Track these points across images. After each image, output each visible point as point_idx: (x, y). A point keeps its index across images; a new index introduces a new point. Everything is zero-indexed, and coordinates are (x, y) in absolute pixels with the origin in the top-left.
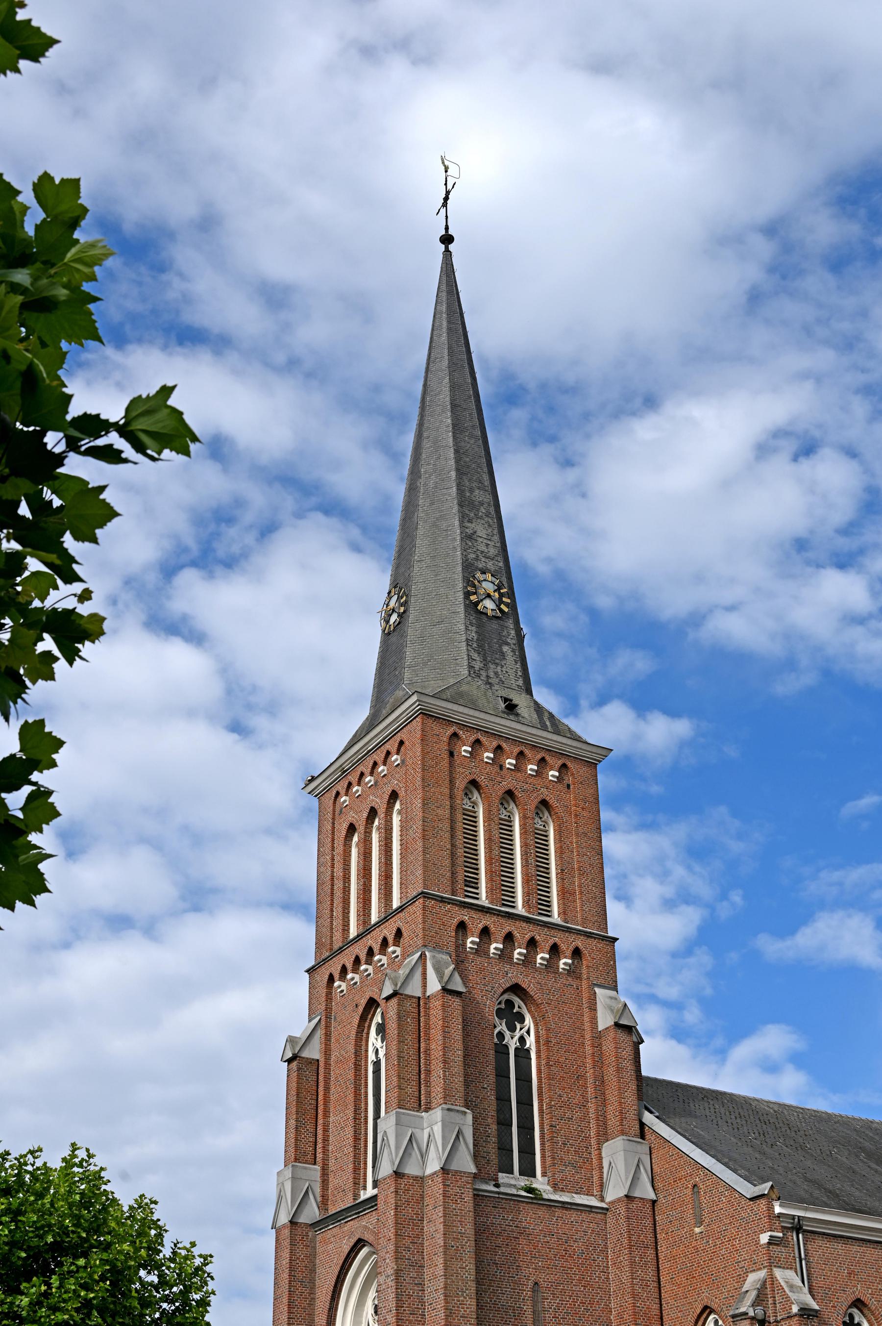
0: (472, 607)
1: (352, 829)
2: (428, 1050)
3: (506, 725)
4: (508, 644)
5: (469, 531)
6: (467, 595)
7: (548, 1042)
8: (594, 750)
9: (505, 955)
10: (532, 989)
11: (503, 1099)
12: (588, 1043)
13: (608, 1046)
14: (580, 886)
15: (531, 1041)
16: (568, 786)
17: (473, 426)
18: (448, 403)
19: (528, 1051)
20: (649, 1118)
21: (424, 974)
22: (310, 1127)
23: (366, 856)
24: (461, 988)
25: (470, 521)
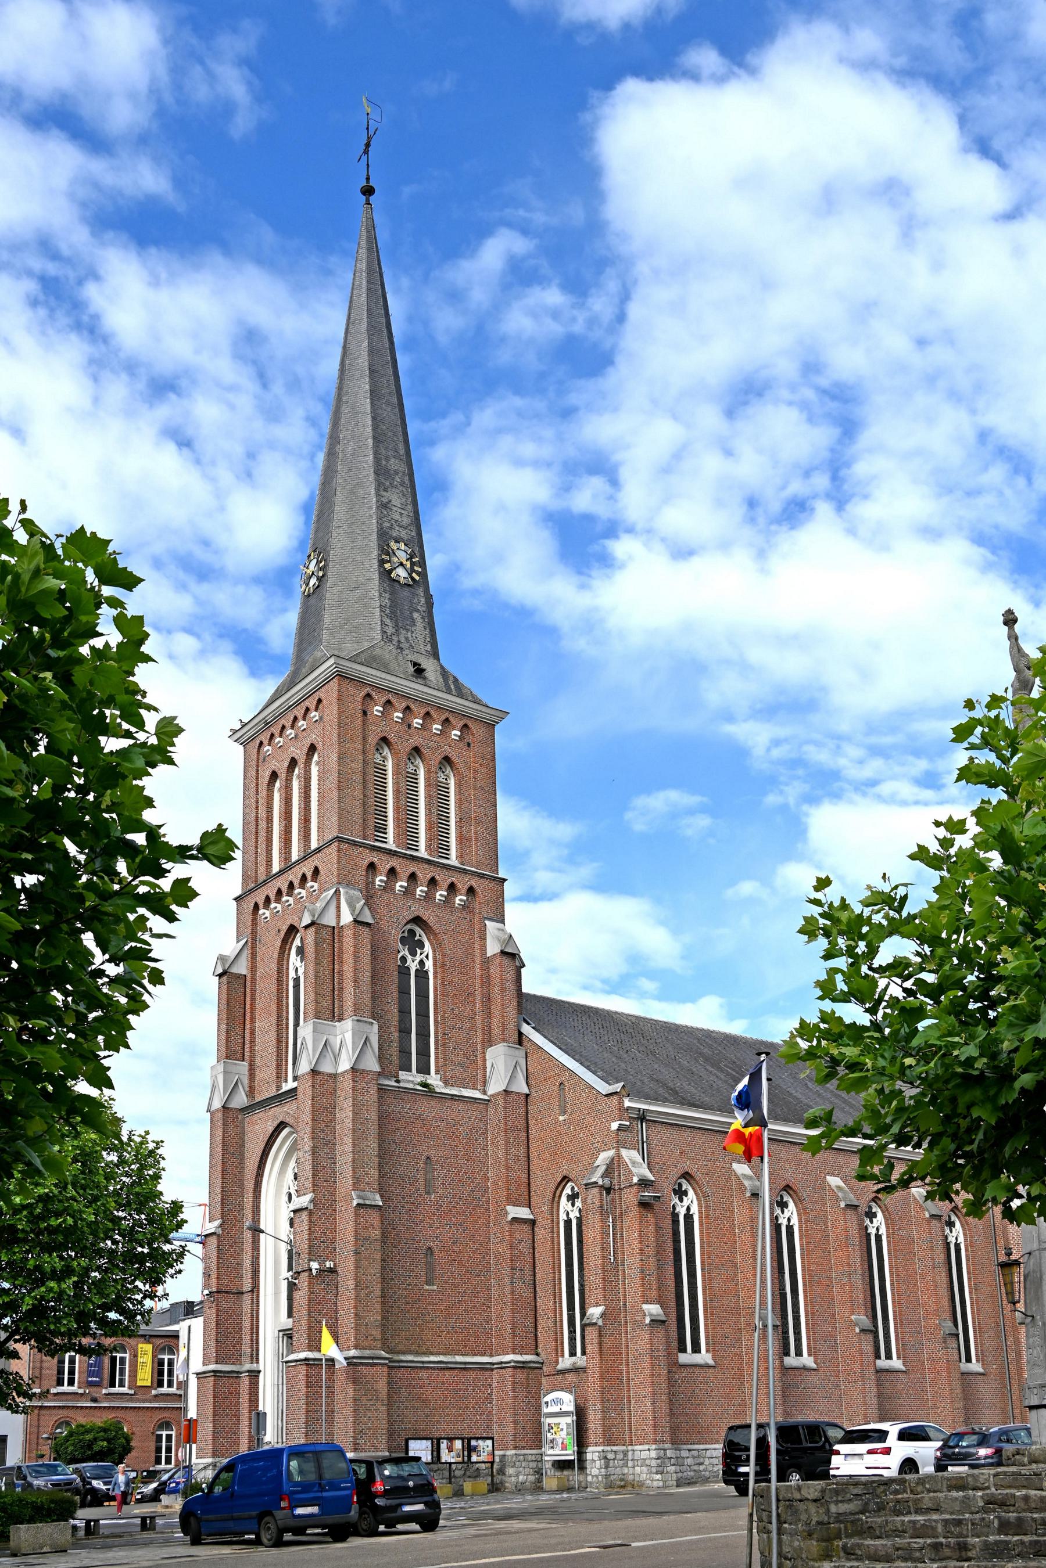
0: (386, 575)
1: (274, 776)
3: (414, 687)
4: (418, 611)
5: (384, 500)
6: (382, 562)
7: (443, 966)
8: (493, 712)
9: (409, 892)
10: (431, 921)
11: (404, 1011)
13: (495, 970)
14: (475, 833)
15: (429, 965)
16: (469, 745)
18: (366, 368)
19: (427, 972)
20: (526, 1029)
22: (239, 1031)
23: (287, 801)
24: (370, 920)
25: (385, 490)
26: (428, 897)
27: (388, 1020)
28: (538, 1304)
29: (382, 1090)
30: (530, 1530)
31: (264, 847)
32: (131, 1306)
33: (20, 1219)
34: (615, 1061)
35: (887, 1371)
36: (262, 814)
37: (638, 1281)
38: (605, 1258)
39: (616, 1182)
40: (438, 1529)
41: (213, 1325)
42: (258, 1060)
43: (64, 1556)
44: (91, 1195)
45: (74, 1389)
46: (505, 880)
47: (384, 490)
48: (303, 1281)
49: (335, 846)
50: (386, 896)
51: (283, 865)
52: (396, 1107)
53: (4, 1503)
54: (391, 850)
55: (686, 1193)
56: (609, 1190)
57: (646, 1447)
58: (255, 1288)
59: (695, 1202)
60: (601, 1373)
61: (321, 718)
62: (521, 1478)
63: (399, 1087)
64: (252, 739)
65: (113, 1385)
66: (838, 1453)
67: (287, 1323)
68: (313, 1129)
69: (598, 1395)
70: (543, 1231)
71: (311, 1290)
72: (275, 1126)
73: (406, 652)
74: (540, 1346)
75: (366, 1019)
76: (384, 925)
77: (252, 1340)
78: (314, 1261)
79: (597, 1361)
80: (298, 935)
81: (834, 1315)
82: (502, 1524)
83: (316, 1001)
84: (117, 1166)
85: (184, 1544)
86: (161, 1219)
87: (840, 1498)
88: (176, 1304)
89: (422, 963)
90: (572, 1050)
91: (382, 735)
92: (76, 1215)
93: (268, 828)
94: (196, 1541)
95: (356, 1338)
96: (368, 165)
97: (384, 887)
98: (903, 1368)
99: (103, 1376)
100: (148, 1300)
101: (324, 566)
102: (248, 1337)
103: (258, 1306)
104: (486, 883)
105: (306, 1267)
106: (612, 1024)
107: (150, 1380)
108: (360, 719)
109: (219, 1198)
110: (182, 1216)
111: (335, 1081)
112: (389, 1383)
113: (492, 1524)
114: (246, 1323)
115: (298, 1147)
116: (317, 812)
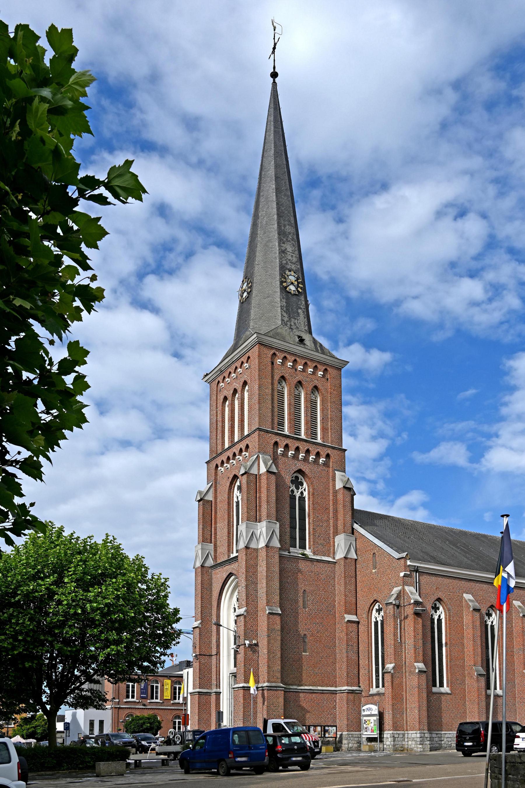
0: (284, 289)
1: (225, 399)
2: (260, 497)
3: (299, 349)
4: (301, 308)
5: (283, 249)
6: (282, 282)
7: (313, 494)
8: (340, 362)
9: (295, 457)
10: (307, 471)
13: (340, 496)
14: (331, 426)
15: (306, 494)
16: (327, 379)
18: (273, 176)
19: (304, 498)
20: (356, 526)
22: (209, 528)
24: (275, 470)
25: (284, 243)
26: (306, 459)
27: (285, 522)
28: (360, 662)
29: (281, 557)
30: (357, 771)
31: (221, 435)
32: (154, 659)
33: (97, 615)
34: (402, 542)
36: (220, 418)
37: (412, 651)
38: (395, 640)
39: (402, 602)
40: (309, 769)
41: (198, 671)
42: (218, 542)
43: (121, 778)
44: (132, 604)
45: (134, 700)
46: (346, 450)
47: (283, 243)
48: (241, 650)
49: (257, 433)
51: (230, 445)
52: (289, 566)
53: (94, 751)
54: (286, 435)
55: (438, 609)
56: (398, 606)
57: (415, 732)
58: (218, 653)
59: (443, 613)
60: (392, 696)
61: (249, 366)
62: (350, 745)
63: (290, 555)
64: (214, 380)
65: (152, 698)
66: (518, 737)
67: (233, 669)
68: (246, 576)
69: (390, 707)
70: (363, 627)
71: (245, 654)
72: (227, 575)
73: (295, 330)
74: (361, 682)
75: (273, 521)
76: (283, 473)
77: (217, 678)
78: (247, 640)
79: (390, 690)
80: (238, 480)
81: (514, 670)
82: (343, 768)
83: (248, 512)
84: (146, 590)
85: (181, 773)
86: (168, 617)
88: (181, 662)
89: (302, 493)
90: (380, 537)
91: (281, 375)
92: (124, 613)
93: (222, 426)
94: (187, 772)
95: (268, 677)
96: (274, 60)
97: (282, 454)
99: (148, 694)
100: (163, 656)
101: (251, 286)
102: (215, 676)
103: (219, 662)
105: (243, 643)
106: (400, 524)
107: (170, 697)
108: (270, 366)
109: (200, 610)
110: (179, 616)
111: (257, 552)
112: (284, 699)
113: (337, 768)
114: (214, 669)
115: (239, 585)
116: (248, 416)
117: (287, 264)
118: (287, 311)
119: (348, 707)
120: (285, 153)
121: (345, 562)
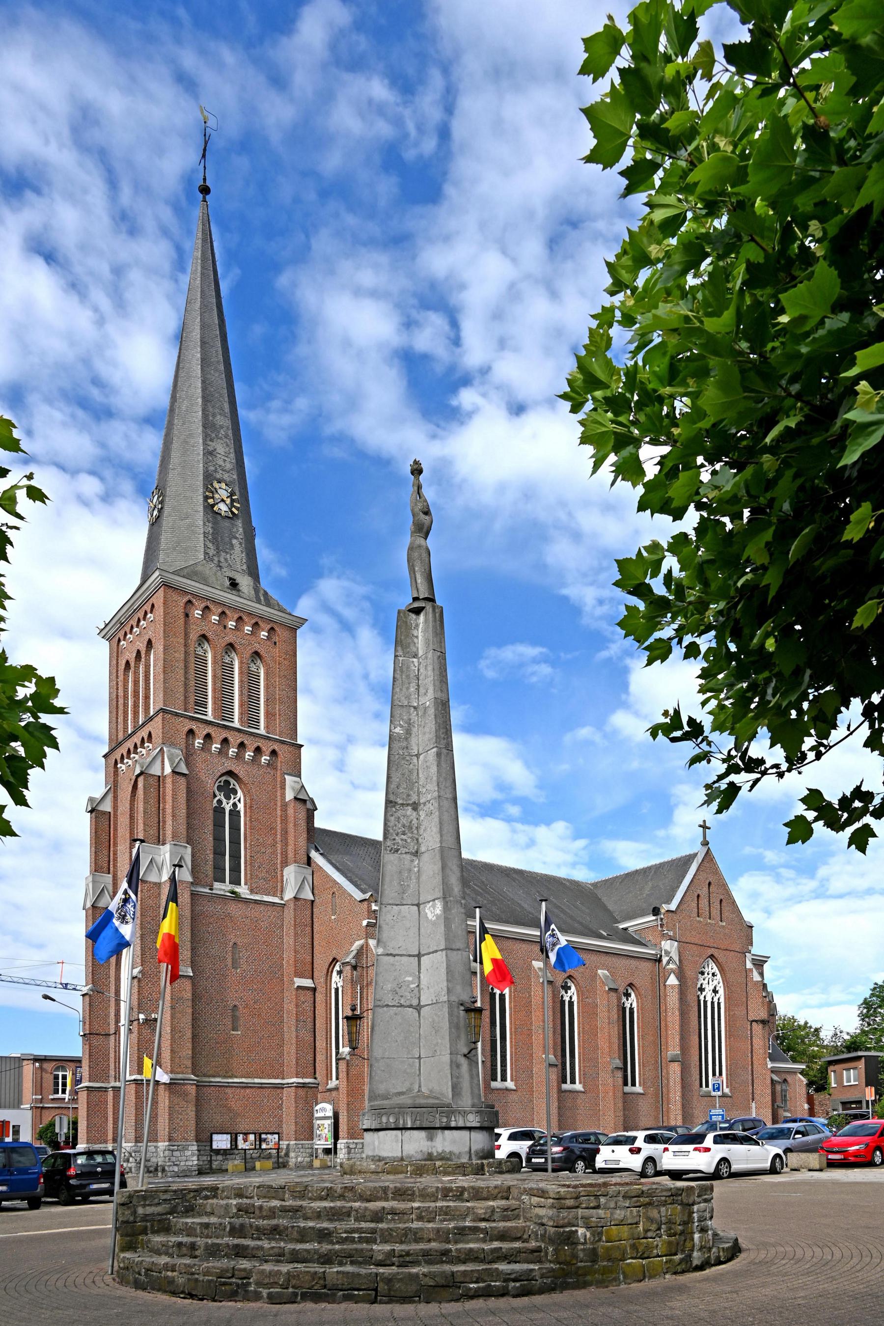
0: (209, 508)
2: (164, 809)
3: (230, 597)
4: (236, 538)
5: (211, 448)
6: (206, 498)
7: (251, 807)
8: (294, 619)
9: (222, 752)
10: (241, 774)
11: (219, 839)
12: (279, 808)
13: (290, 811)
14: (279, 710)
15: (241, 807)
16: (275, 643)
17: (218, 362)
18: (199, 340)
19: (239, 812)
20: (314, 854)
21: (163, 762)
22: (105, 852)
23: (136, 683)
24: (185, 771)
25: (211, 440)
29: (194, 895)
35: (570, 1091)
50: (204, 754)
60: (348, 1091)
69: (345, 1106)
70: (320, 996)
73: (225, 570)
74: (317, 1073)
81: (532, 1055)
87: (147, 1203)
89: (235, 805)
91: (202, 633)
98: (583, 1090)
104: (286, 747)
117: (216, 471)
118: (214, 541)
119: (296, 1107)
120: (217, 307)
121: (295, 905)
